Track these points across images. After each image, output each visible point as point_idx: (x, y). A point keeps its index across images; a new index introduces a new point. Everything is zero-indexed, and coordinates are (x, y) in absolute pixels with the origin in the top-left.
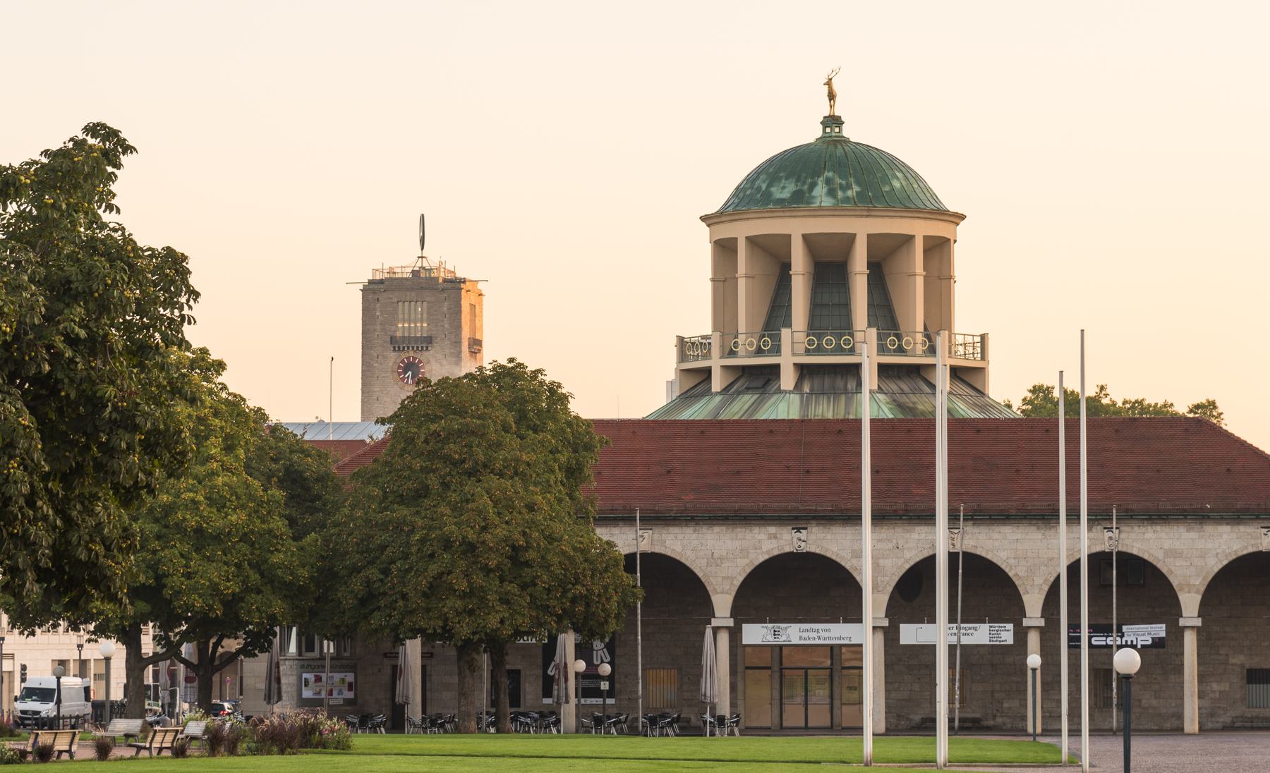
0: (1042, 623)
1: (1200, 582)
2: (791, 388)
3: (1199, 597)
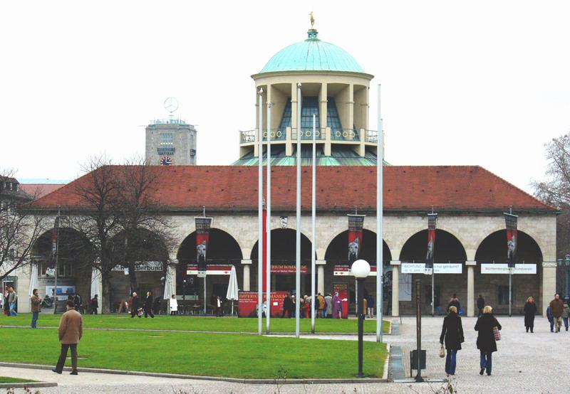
0: (250, 262)
1: (476, 244)
2: (291, 155)
3: (475, 252)
